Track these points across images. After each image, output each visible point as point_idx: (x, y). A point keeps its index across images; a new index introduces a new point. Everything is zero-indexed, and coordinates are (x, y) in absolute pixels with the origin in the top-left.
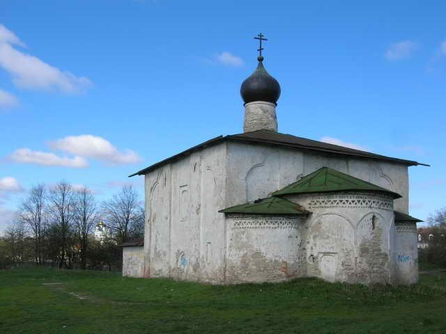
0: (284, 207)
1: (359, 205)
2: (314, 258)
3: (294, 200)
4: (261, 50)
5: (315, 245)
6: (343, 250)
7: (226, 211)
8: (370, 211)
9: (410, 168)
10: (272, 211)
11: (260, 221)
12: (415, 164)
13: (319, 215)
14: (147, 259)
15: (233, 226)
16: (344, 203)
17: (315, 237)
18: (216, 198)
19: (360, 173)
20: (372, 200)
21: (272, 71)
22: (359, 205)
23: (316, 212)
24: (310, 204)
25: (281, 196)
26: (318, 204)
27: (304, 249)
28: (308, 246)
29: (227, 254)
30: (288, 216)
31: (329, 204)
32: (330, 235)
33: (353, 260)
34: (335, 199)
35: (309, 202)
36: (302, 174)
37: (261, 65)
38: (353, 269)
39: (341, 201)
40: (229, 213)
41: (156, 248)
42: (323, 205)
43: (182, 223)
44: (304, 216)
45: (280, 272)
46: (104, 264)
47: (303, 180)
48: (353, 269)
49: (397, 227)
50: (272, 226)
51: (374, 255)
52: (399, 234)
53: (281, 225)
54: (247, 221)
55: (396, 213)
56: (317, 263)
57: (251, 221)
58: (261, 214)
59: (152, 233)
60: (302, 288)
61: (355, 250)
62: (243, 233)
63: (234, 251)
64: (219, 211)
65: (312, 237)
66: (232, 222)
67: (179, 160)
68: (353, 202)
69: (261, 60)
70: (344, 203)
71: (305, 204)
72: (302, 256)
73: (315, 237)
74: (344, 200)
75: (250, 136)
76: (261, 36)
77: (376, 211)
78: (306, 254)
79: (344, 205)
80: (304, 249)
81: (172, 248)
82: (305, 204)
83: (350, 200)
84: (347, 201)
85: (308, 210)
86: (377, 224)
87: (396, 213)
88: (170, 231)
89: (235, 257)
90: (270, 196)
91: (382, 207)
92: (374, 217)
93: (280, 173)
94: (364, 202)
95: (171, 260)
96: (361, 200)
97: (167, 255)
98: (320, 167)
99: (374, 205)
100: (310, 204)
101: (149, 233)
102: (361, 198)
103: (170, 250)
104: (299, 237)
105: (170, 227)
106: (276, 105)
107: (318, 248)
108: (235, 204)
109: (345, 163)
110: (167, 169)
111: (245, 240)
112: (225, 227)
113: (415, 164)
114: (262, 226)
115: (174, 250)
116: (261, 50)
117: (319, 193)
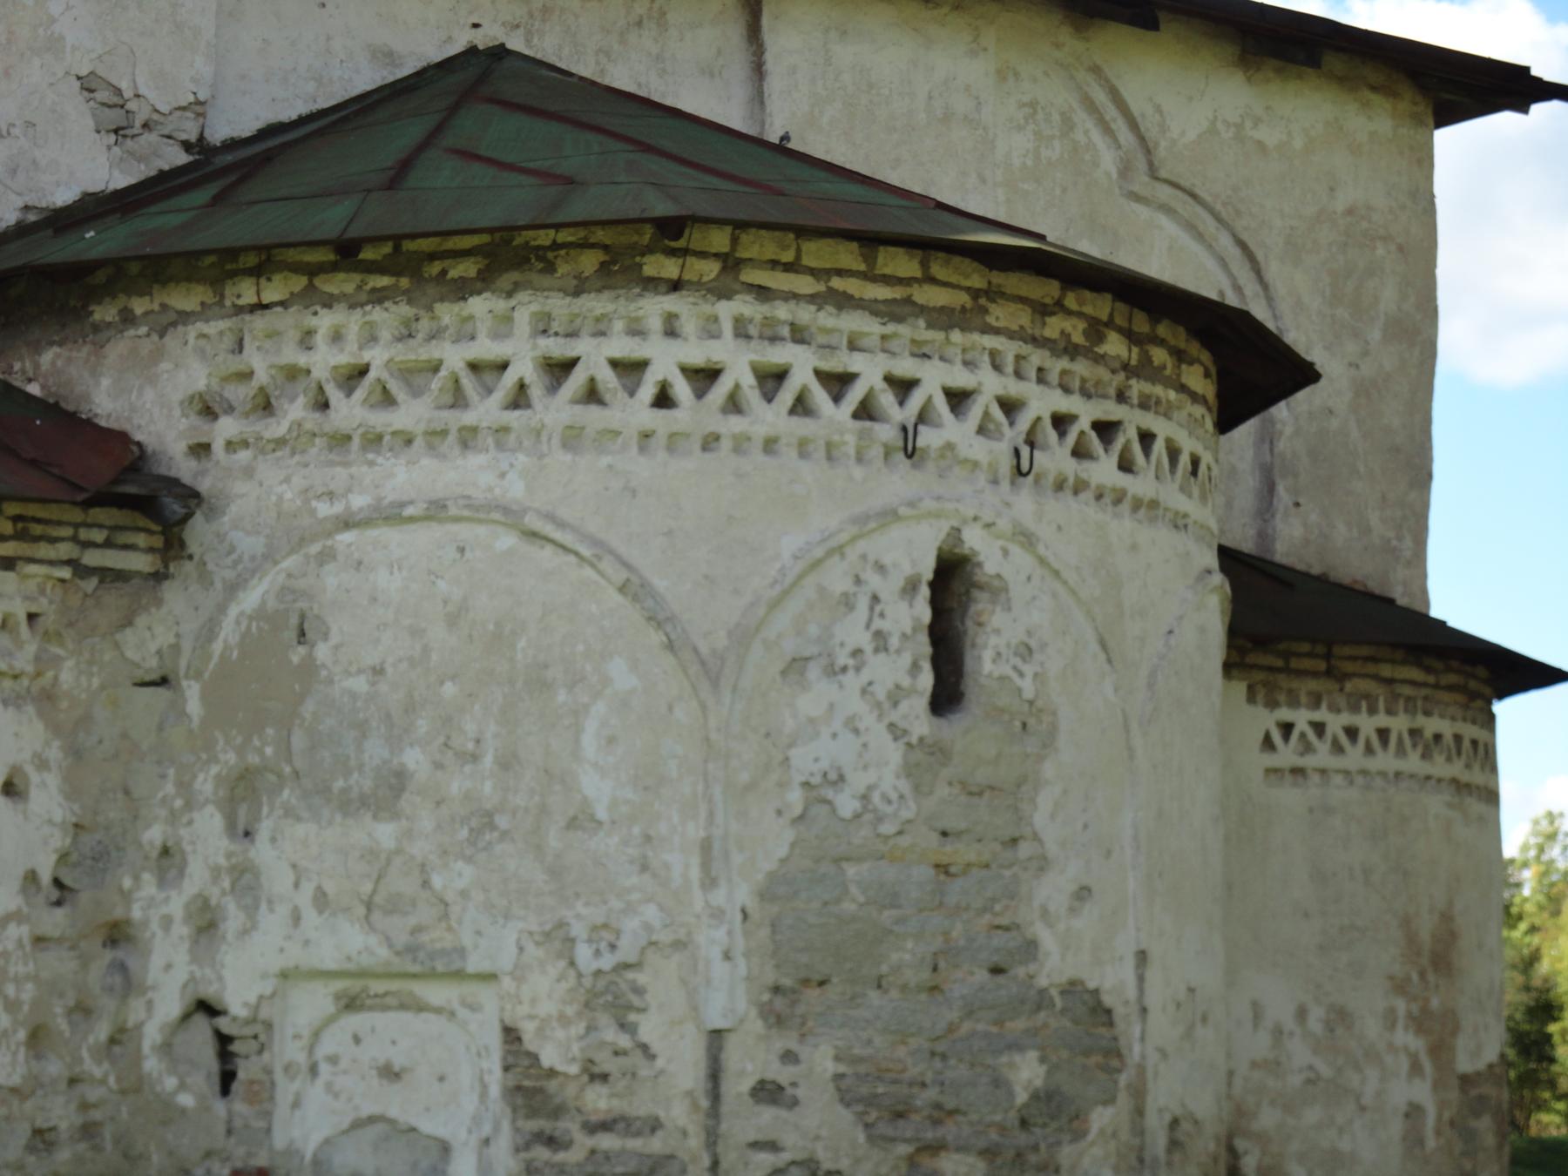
2: (224, 1040)
5: (244, 879)
6: (559, 939)
8: (899, 483)
12: (1510, 87)
16: (664, 400)
22: (770, 417)
23: (256, 496)
26: (295, 410)
28: (158, 909)
31: (412, 414)
32: (414, 759)
33: (682, 1064)
34: (486, 348)
36: (198, 107)
39: (560, 369)
42: (349, 411)
49: (1265, 720)
52: (1289, 796)
56: (263, 1094)
61: (711, 940)
64: (511, 1035)
65: (205, 784)
68: (704, 377)
70: (592, 395)
72: (83, 1011)
73: (243, 798)
78: (127, 983)
79: (593, 416)
80: (117, 934)
84: (630, 369)
85: (185, 469)
86: (990, 655)
91: (1055, 458)
92: (951, 580)
94: (838, 383)
99: (950, 431)
102: (799, 335)
107: (272, 923)
113: (1510, 87)
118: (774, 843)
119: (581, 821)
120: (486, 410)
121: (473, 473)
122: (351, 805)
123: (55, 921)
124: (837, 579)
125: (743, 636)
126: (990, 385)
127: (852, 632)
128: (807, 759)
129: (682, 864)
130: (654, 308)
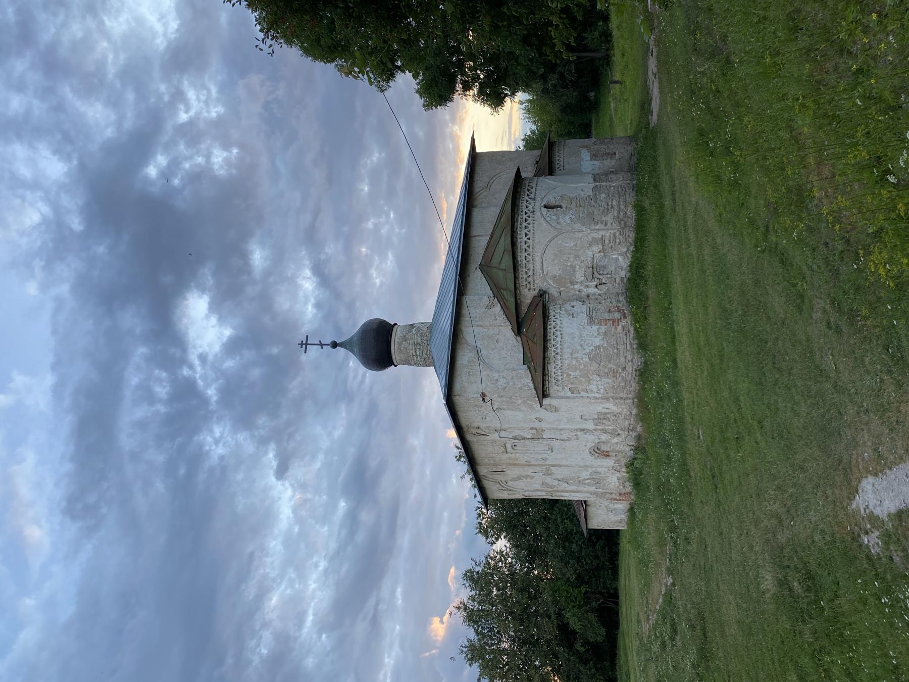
0: (531, 321)
1: (531, 227)
3: (524, 309)
4: (321, 345)
7: (541, 396)
8: (538, 213)
9: (478, 150)
10: (539, 340)
11: (553, 354)
13: (544, 279)
14: (602, 495)
15: (560, 388)
17: (572, 283)
18: (523, 408)
19: (487, 216)
20: (525, 210)
21: (352, 328)
23: (539, 283)
24: (529, 289)
25: (519, 328)
27: (588, 296)
29: (597, 395)
30: (545, 317)
31: (531, 266)
35: (526, 290)
37: (342, 345)
38: (615, 235)
40: (543, 394)
41: (589, 484)
42: (530, 273)
43: (555, 451)
44: (542, 300)
45: (620, 328)
46: (529, 571)
47: (497, 291)
48: (615, 235)
50: (559, 339)
51: (596, 205)
52: (566, 167)
53: (558, 328)
54: (554, 370)
55: (538, 174)
57: (553, 365)
58: (544, 369)
59: (476, 214)
60: (641, 293)
62: (568, 375)
63: (593, 387)
66: (553, 389)
67: (472, 455)
68: (526, 235)
69: (335, 345)
71: (528, 295)
73: (572, 283)
74: (524, 246)
75: (444, 372)
76: (302, 344)
77: (538, 204)
78: (594, 294)
80: (588, 296)
81: (588, 463)
82: (528, 295)
83: (525, 239)
85: (537, 291)
86: (553, 202)
87: (538, 174)
88: (566, 466)
89: (599, 385)
90: (519, 338)
91: (532, 196)
92: (546, 207)
93: (490, 327)
94: (526, 220)
95: (605, 464)
96: (524, 224)
97: (599, 470)
98: (479, 273)
99: (530, 208)
100: (529, 289)
101: (476, 230)
103: (591, 467)
104: (574, 303)
105: (560, 466)
106: (395, 324)
108: (531, 385)
109: (474, 239)
110: (482, 470)
111: (578, 373)
112: (562, 397)
113: (473, 141)
114: (559, 351)
115: (590, 460)
116: (321, 345)
117: (516, 278)
118: (578, 226)
119: (576, 245)
120: (531, 258)
121: (538, 259)
122: (574, 271)
123: (587, 302)
124: (548, 219)
125: (555, 228)
126: (525, 203)
127: (554, 217)
128: (569, 221)
129: (580, 235)
130: (519, 240)
